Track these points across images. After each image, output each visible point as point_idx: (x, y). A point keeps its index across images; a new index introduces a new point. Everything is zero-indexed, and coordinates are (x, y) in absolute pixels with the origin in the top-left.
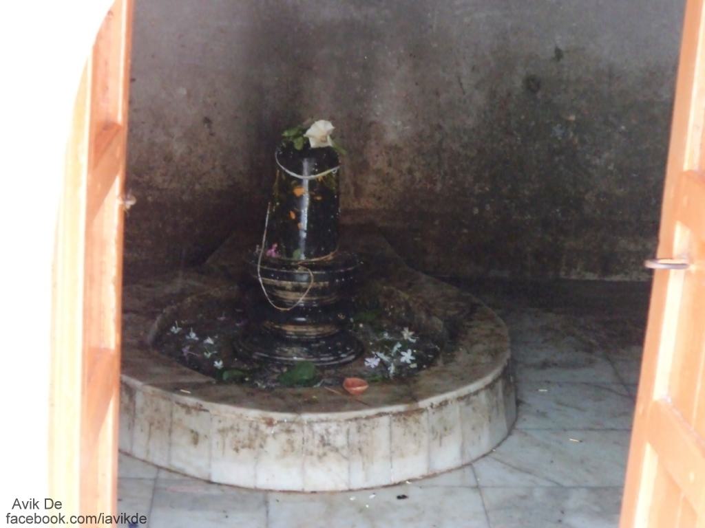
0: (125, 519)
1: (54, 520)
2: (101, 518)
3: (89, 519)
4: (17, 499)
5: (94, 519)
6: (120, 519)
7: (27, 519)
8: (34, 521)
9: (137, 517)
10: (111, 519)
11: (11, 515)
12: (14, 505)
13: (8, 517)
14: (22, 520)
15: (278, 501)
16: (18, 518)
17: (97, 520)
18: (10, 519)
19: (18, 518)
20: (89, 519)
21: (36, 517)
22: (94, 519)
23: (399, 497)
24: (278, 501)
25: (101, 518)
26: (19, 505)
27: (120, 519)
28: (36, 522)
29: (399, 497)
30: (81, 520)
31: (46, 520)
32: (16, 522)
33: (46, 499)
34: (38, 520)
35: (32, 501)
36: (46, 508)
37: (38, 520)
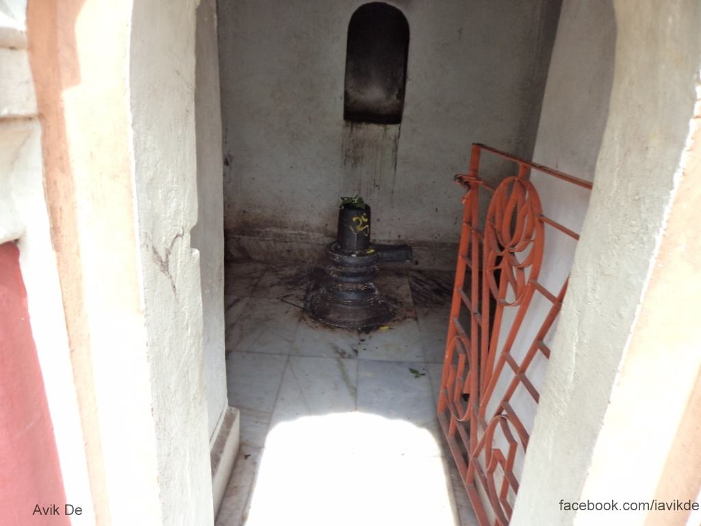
0: (54, 511)
1: (607, 506)
2: (654, 504)
3: (642, 505)
4: (37, 505)
5: (646, 505)
6: (49, 509)
7: (580, 506)
8: (587, 507)
9: (689, 504)
10: (664, 506)
11: (564, 502)
12: (35, 511)
13: (561, 503)
14: (575, 506)
15: (437, 210)
16: (571, 504)
17: (650, 507)
18: (563, 506)
19: (571, 504)
20: (642, 505)
21: (589, 504)
22: (646, 505)
23: (91, 153)
24: (437, 210)
25: (654, 504)
26: (40, 511)
27: (49, 509)
28: (589, 509)
29: (91, 153)
30: (634, 506)
31: (599, 506)
32: (570, 509)
33: (66, 514)
34: (591, 506)
35: (52, 507)
36: (66, 514)
37: (591, 506)
